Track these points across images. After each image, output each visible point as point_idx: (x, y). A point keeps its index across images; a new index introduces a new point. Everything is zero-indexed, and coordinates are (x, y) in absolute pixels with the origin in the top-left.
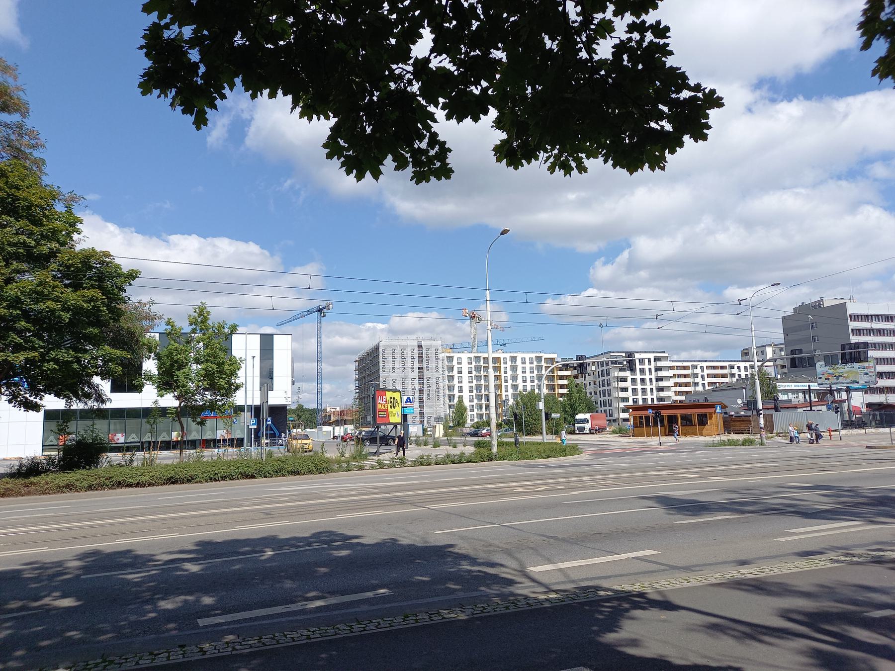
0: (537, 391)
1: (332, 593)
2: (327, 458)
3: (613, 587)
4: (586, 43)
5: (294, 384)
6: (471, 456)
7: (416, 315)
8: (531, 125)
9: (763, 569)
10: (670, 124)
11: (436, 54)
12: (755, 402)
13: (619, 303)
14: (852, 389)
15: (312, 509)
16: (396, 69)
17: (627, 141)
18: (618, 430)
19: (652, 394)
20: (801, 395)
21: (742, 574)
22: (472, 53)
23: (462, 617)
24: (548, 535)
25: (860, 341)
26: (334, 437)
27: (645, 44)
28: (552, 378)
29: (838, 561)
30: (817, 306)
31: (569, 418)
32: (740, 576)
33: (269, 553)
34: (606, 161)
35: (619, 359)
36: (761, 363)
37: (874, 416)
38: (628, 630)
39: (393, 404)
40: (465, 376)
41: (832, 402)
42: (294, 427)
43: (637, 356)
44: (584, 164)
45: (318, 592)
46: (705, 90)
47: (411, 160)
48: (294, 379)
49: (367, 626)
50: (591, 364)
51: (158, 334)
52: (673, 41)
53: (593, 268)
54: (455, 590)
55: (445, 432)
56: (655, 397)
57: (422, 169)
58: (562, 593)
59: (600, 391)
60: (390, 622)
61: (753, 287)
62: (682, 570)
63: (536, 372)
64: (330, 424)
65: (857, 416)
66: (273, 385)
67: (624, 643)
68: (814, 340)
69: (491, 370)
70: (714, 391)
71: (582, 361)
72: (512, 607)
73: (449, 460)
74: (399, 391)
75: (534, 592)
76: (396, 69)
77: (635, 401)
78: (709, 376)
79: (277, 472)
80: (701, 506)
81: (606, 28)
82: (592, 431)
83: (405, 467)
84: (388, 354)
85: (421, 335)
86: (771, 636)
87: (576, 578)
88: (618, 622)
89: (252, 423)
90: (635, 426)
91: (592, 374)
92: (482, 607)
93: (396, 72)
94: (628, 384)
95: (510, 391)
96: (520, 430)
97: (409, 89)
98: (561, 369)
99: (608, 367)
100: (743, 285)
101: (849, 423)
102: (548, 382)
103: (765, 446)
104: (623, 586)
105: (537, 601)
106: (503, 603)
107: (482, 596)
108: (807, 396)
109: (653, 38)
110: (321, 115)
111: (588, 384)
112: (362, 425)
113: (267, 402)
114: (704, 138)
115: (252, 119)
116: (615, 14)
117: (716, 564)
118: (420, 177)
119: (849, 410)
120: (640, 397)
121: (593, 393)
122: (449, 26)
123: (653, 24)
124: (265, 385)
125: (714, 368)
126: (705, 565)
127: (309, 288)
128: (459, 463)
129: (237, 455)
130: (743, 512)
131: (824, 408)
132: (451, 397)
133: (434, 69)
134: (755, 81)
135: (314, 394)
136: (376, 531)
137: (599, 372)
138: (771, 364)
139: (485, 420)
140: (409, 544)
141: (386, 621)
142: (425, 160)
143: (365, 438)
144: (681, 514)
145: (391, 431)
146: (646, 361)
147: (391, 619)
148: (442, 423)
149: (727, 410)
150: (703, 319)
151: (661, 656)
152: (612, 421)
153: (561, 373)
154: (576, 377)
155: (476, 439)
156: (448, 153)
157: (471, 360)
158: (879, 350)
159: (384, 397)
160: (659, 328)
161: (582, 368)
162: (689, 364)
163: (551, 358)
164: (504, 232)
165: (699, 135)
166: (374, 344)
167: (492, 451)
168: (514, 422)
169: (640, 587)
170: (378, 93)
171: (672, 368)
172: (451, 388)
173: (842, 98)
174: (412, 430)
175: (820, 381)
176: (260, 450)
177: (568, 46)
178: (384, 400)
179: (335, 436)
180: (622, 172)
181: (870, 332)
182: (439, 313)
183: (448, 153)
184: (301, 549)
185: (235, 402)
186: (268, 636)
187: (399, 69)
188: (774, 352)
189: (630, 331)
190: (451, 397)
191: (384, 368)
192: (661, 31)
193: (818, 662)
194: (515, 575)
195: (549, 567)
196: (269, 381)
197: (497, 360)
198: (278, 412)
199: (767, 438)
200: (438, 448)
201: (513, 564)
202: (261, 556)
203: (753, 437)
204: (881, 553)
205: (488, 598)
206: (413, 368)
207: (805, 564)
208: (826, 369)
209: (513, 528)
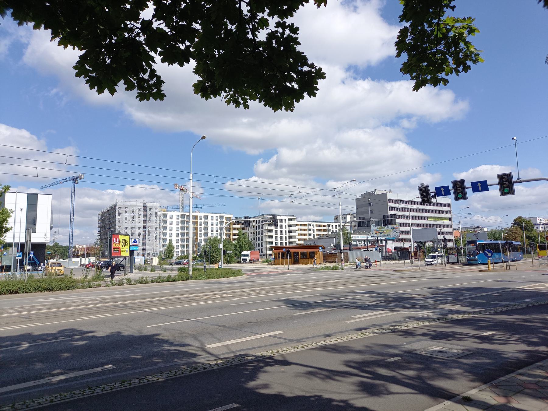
0: (219, 237)
1: (71, 370)
3: (256, 354)
5: (52, 229)
6: (175, 277)
7: (142, 186)
9: (338, 339)
10: (297, 85)
11: (156, 19)
12: (340, 246)
13: (270, 186)
14: (388, 239)
15: (61, 314)
16: (129, 24)
17: (273, 92)
18: (266, 261)
19: (286, 240)
20: (363, 242)
22: (181, 23)
25: (392, 214)
26: (81, 265)
27: (285, 36)
29: (375, 333)
30: (373, 194)
31: (238, 254)
32: (326, 344)
33: (25, 345)
34: (260, 102)
35: (268, 219)
36: (344, 224)
37: (398, 253)
38: (262, 379)
39: (124, 244)
40: (174, 226)
41: (378, 246)
42: (51, 259)
43: (279, 218)
45: (61, 370)
46: (316, 68)
47: (137, 85)
48: (52, 225)
49: (95, 390)
50: (252, 221)
52: (301, 36)
53: (256, 165)
54: (158, 362)
56: (287, 242)
58: (226, 360)
59: (257, 238)
60: (111, 386)
61: (341, 181)
62: (295, 341)
63: (219, 225)
64: (78, 257)
65: (389, 254)
67: (260, 387)
68: (371, 212)
69: (191, 223)
70: (319, 239)
71: (247, 220)
72: (194, 370)
73: (161, 280)
74: (129, 235)
75: (208, 361)
77: (276, 244)
78: (317, 230)
79: (35, 289)
80: (308, 304)
81: (264, 23)
82: (251, 262)
83: (130, 284)
85: (145, 199)
86: (339, 376)
88: (257, 375)
89: (18, 255)
90: (275, 258)
91: (252, 227)
92: (175, 372)
93: (129, 26)
94: (273, 234)
95: (203, 237)
96: (207, 261)
97: (137, 38)
98: (234, 224)
99: (262, 224)
100: (337, 180)
102: (227, 232)
103: (343, 270)
104: (261, 353)
106: (188, 368)
107: (175, 365)
108: (366, 243)
111: (250, 233)
112: (102, 257)
113: (30, 240)
114: (315, 95)
115: (28, 44)
116: (269, 15)
117: (314, 337)
118: (142, 97)
119: (386, 250)
120: (279, 242)
121: (253, 239)
122: (166, 3)
123: (290, 25)
124: (29, 229)
125: (320, 226)
126: (308, 338)
127: (66, 164)
129: (5, 277)
130: (329, 307)
131: (374, 249)
133: (155, 29)
134: (347, 67)
137: (257, 226)
138: (349, 224)
139: (186, 255)
141: (109, 386)
143: (103, 266)
144: (297, 309)
145: (122, 261)
146: (284, 221)
147: (113, 384)
149: (325, 250)
150: (315, 198)
151: (279, 393)
154: (243, 229)
155: (179, 266)
156: (162, 84)
157: (179, 217)
158: (402, 219)
159: (118, 239)
160: (291, 202)
161: (247, 224)
162: (307, 223)
163: (229, 217)
164: (203, 138)
165: (312, 94)
167: (189, 274)
168: (204, 256)
169: (271, 353)
171: (297, 225)
172: (165, 234)
173: (389, 82)
174: (137, 261)
175: (372, 235)
176: (23, 274)
177: (242, 29)
178: (118, 241)
179: (82, 265)
180: (269, 109)
181: (398, 209)
182: (159, 186)
183: (162, 84)
185: (4, 240)
186: (19, 403)
187: (131, 25)
188: (351, 218)
189: (275, 203)
190: (164, 240)
191: (119, 220)
192: (295, 30)
193: (361, 389)
194: (197, 351)
195: (219, 344)
196: (33, 226)
197: (195, 217)
198: (39, 248)
200: (154, 272)
202: (19, 348)
203: (338, 265)
204: (396, 327)
205: (178, 366)
206: (139, 220)
207: (359, 335)
208: (376, 228)
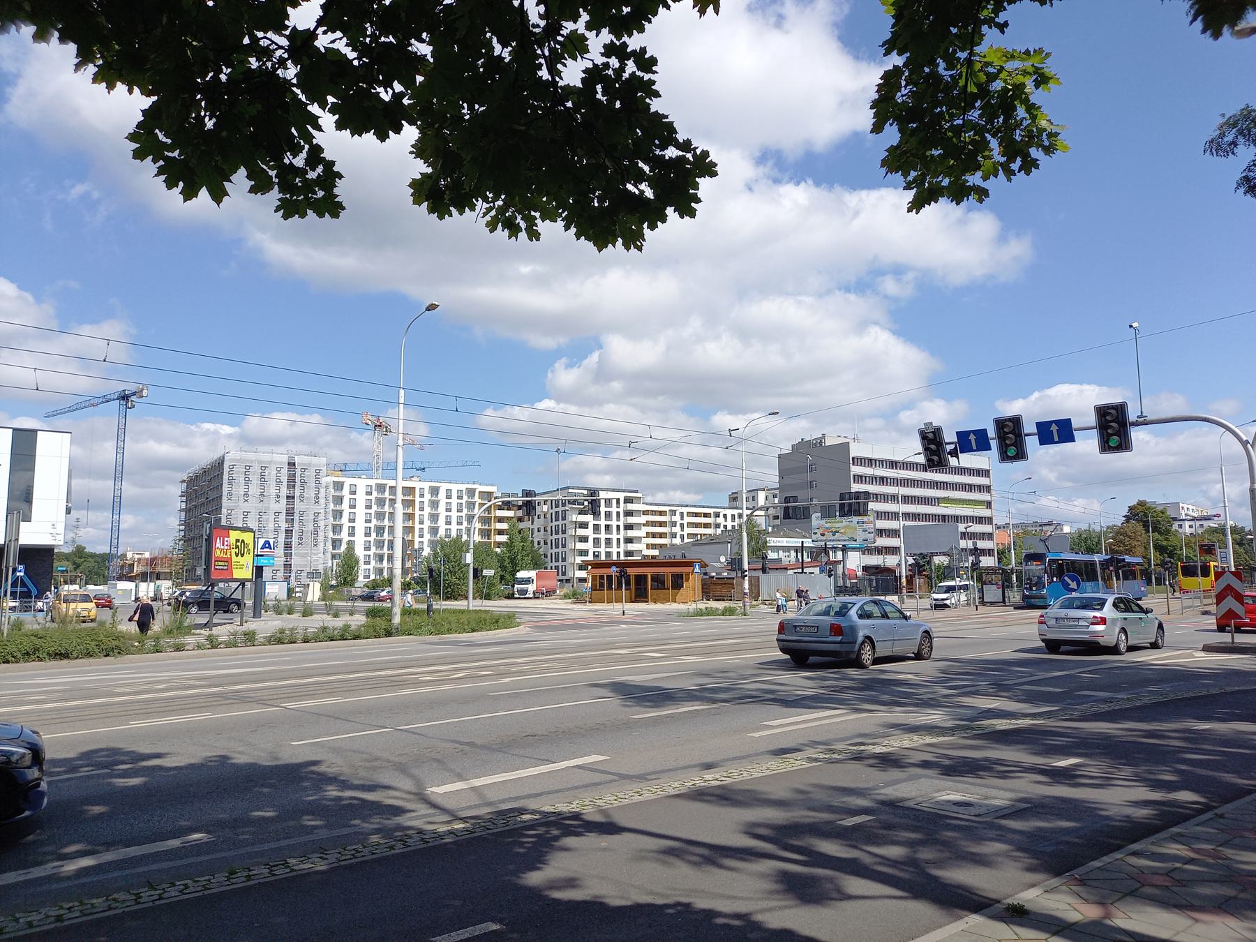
0: (465, 538)
2: (120, 632)
3: (543, 809)
4: (548, 58)
5: (69, 513)
8: (465, 159)
9: (731, 773)
11: (326, 28)
12: (740, 561)
13: (583, 422)
14: (849, 548)
16: (262, 38)
17: (596, 204)
19: (618, 546)
20: (793, 553)
21: (706, 781)
22: (383, 39)
23: (322, 866)
24: (461, 740)
25: (860, 490)
27: (626, 75)
28: (487, 521)
29: (816, 760)
30: (818, 444)
32: (703, 784)
34: (567, 228)
35: (579, 498)
37: (870, 580)
40: (360, 511)
41: (826, 564)
42: (66, 583)
43: (603, 495)
44: (537, 226)
47: (277, 181)
48: (70, 505)
49: (165, 892)
50: (542, 503)
51: (11, 430)
54: (316, 827)
55: (323, 594)
56: (621, 550)
57: (295, 197)
58: (473, 821)
59: (552, 540)
63: (465, 511)
64: (130, 579)
65: (852, 581)
66: (31, 512)
69: (399, 505)
70: (694, 544)
71: (595, 498)
72: (399, 845)
73: (327, 636)
74: (252, 531)
76: (262, 38)
77: (596, 555)
78: (691, 525)
79: (28, 654)
80: (665, 694)
81: (577, 46)
83: (253, 645)
84: (238, 472)
87: (495, 799)
90: (594, 588)
91: (542, 517)
92: (354, 850)
94: (589, 532)
95: (427, 537)
96: (436, 592)
97: (280, 72)
98: (500, 508)
99: (564, 508)
101: (843, 589)
102: (482, 526)
104: (556, 805)
105: (436, 835)
108: (799, 555)
109: (635, 69)
110: (135, 87)
112: (187, 582)
113: (17, 540)
114: (692, 213)
117: (677, 769)
118: (289, 209)
120: (602, 550)
121: (542, 543)
123: (636, 50)
124: (15, 512)
125: (697, 515)
126: (663, 771)
127: (105, 361)
128: (340, 640)
130: (714, 701)
131: (817, 570)
132: (336, 543)
134: (758, 154)
135: (107, 530)
136: (194, 744)
137: (552, 514)
138: (762, 513)
139: (386, 577)
140: (247, 763)
141: (198, 881)
142: (300, 184)
143: (190, 601)
145: (235, 591)
146: (614, 502)
147: (207, 878)
148: (320, 580)
149: (708, 570)
150: (685, 451)
152: (564, 581)
153: (500, 513)
154: (520, 520)
155: (370, 604)
156: (337, 179)
157: (371, 489)
158: (881, 502)
159: (226, 539)
160: (631, 460)
161: (529, 508)
162: (667, 509)
164: (431, 307)
165: (686, 210)
166: (219, 455)
168: (428, 581)
170: (229, 70)
171: (645, 513)
172: (337, 529)
173: (855, 190)
175: (814, 537)
177: (525, 56)
178: (226, 543)
180: (587, 246)
183: (337, 179)
184: (61, 777)
187: (265, 40)
188: (767, 498)
189: (595, 461)
190: (336, 543)
191: (230, 494)
192: (647, 63)
194: (408, 800)
196: (24, 506)
199: (751, 607)
201: (407, 784)
202: (1043, 739)
203: (735, 605)
204: (862, 748)
205: (362, 837)
208: (823, 522)
209: (413, 733)
